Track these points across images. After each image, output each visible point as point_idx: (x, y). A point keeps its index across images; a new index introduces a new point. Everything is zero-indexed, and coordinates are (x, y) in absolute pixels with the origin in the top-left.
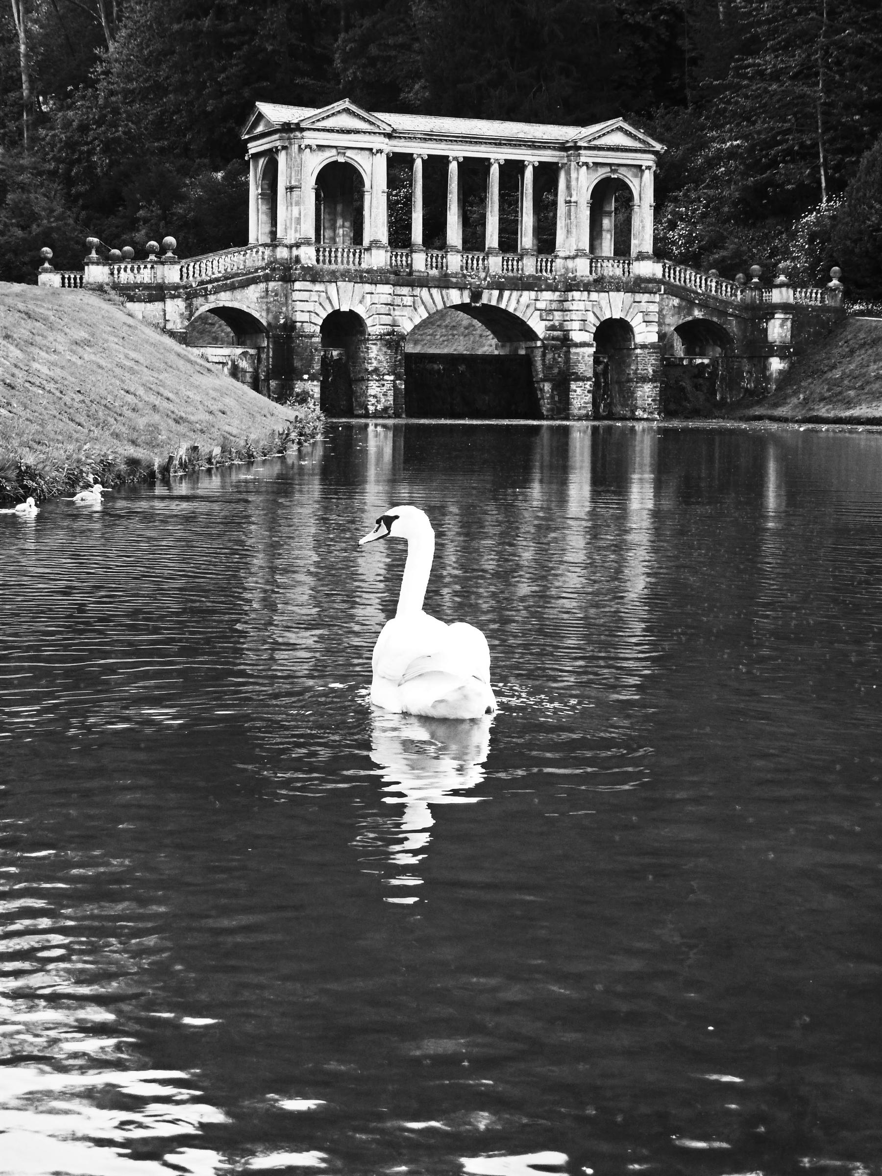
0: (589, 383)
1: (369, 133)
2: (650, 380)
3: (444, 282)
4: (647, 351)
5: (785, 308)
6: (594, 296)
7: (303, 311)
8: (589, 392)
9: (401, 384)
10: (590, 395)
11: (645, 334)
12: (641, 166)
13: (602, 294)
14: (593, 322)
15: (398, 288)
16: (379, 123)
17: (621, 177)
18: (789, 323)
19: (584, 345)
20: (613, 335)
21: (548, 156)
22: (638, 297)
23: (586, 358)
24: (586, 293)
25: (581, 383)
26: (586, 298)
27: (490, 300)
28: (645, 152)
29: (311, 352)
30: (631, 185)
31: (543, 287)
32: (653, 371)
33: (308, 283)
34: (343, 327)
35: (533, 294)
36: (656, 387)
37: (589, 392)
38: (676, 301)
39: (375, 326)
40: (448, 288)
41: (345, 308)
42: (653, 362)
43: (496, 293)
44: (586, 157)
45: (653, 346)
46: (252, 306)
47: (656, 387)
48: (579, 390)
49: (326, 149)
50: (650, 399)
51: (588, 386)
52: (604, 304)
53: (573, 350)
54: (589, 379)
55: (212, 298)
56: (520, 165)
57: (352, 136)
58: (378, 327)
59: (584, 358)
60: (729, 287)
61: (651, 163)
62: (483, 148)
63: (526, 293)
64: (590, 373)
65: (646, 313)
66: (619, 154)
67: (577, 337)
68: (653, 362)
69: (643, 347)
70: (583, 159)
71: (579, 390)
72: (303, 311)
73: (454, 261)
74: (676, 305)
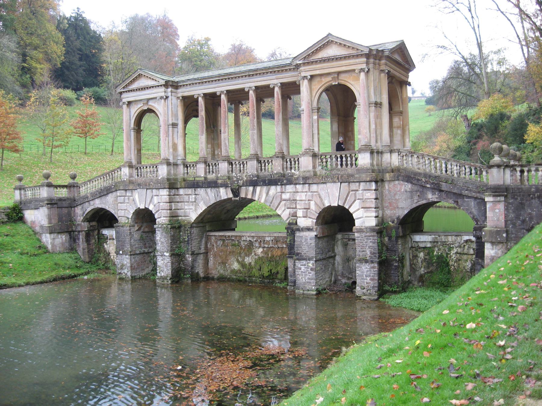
0: (312, 262)
1: (156, 86)
2: (366, 261)
3: (213, 184)
4: (363, 235)
5: (499, 191)
6: (314, 187)
7: (122, 210)
8: (312, 269)
9: (189, 257)
10: (313, 273)
11: (364, 218)
12: (354, 70)
13: (321, 186)
14: (315, 209)
15: (186, 189)
16: (157, 79)
17: (343, 82)
18: (501, 207)
19: (309, 229)
20: (336, 221)
21: (288, 77)
22: (354, 186)
23: (309, 241)
24: (307, 185)
25: (304, 262)
26: (307, 190)
27: (246, 194)
28: (357, 56)
29: (124, 236)
30: (352, 88)
31: (285, 181)
32: (371, 253)
33: (123, 191)
34: (145, 217)
35: (279, 188)
36: (373, 267)
37: (312, 269)
38: (409, 186)
39: (162, 219)
40: (218, 187)
41: (142, 207)
42: (371, 244)
43: (251, 188)
44: (306, 71)
45: (372, 229)
46: (110, 207)
47: (373, 267)
48: (303, 268)
49: (139, 102)
50: (368, 278)
51: (310, 265)
52: (323, 194)
53: (298, 234)
54: (310, 259)
55: (92, 202)
56: (208, 97)
57: (147, 92)
58: (163, 218)
59: (307, 241)
60: (473, 168)
61: (364, 66)
62: (240, 81)
63: (273, 188)
64: (312, 253)
65: (363, 200)
66: (335, 63)
67: (302, 222)
68: (371, 244)
69: (360, 231)
70: (303, 74)
71: (303, 268)
72: (122, 210)
73: (223, 167)
74: (408, 190)
